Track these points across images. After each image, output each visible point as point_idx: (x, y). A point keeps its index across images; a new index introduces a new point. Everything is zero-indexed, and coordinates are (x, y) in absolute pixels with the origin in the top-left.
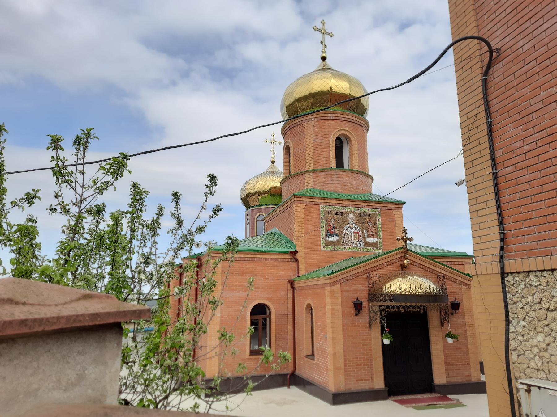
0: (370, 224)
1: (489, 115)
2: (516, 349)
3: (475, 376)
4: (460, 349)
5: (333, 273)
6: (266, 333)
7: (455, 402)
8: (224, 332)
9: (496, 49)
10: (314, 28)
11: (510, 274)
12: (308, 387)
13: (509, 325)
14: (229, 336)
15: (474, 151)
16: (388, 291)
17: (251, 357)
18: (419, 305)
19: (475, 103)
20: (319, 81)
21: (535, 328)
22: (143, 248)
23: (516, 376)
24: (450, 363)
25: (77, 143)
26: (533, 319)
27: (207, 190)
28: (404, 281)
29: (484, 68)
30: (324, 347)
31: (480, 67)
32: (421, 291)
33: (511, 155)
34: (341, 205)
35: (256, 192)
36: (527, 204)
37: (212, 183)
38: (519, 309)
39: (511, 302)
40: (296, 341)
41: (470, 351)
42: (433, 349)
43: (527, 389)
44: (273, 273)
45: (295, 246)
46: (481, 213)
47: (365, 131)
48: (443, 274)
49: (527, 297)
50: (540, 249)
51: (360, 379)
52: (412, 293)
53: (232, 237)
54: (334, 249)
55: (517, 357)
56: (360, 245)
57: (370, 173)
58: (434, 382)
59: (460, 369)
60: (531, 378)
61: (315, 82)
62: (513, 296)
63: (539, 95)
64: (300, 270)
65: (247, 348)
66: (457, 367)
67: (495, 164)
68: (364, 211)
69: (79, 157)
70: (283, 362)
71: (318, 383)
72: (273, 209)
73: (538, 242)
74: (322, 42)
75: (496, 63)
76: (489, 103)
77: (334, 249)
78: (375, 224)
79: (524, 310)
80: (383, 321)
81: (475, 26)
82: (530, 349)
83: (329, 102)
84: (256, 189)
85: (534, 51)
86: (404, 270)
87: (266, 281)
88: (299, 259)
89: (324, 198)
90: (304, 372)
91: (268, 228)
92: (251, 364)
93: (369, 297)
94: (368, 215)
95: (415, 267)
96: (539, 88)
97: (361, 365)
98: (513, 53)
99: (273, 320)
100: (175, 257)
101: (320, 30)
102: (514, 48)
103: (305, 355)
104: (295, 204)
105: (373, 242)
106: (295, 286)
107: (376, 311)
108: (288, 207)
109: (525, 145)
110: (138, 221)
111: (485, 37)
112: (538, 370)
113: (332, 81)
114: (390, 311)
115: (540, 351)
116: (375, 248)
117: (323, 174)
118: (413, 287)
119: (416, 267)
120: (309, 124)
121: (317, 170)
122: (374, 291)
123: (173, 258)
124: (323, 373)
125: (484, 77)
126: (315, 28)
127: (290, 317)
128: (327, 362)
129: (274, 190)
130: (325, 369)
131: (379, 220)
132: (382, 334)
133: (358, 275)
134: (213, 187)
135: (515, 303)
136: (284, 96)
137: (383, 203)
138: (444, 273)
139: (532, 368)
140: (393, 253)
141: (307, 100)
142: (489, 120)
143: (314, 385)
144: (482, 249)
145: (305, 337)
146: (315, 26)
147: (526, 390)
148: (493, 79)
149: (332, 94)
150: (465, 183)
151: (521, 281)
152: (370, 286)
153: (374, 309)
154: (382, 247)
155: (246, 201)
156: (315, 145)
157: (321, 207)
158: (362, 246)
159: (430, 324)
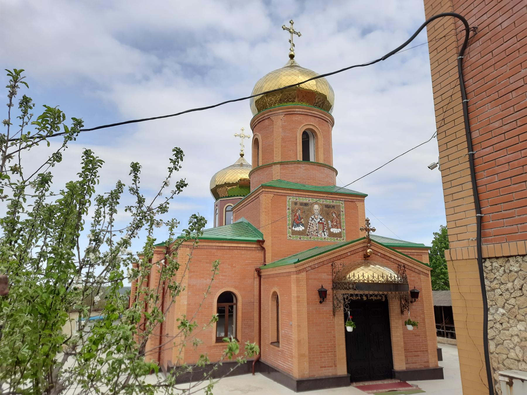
0: (334, 215)
1: (465, 95)
2: (494, 339)
3: (433, 361)
4: (419, 336)
5: (299, 261)
6: (232, 320)
7: (415, 388)
8: (184, 320)
9: (473, 27)
10: (283, 27)
11: (488, 260)
12: (273, 374)
13: (487, 313)
14: (189, 325)
15: (448, 133)
16: (352, 280)
17: (217, 344)
18: (381, 293)
19: (450, 83)
20: (287, 77)
21: (516, 316)
22: (96, 225)
23: (493, 367)
24: (409, 350)
25: (24, 104)
26: (513, 307)
27: (172, 165)
28: (366, 269)
29: (460, 48)
30: (289, 334)
31: (456, 47)
32: (383, 280)
33: (489, 135)
34: (307, 196)
35: (226, 184)
36: (507, 186)
37: (178, 158)
38: (497, 296)
39: (489, 289)
40: (262, 329)
41: (428, 338)
42: (393, 336)
43: (508, 381)
44: (240, 261)
45: (262, 235)
46: (456, 196)
47: (330, 126)
48: (404, 263)
49: (507, 283)
50: (520, 232)
51: (323, 366)
52: (375, 282)
53: (197, 215)
54: (300, 238)
55: (495, 346)
56: (325, 235)
57: (334, 166)
58: (394, 368)
59: (418, 356)
60: (511, 369)
61: (284, 78)
62: (491, 282)
63: (520, 73)
64: (266, 258)
65: (213, 336)
66: (416, 354)
67: (472, 146)
68: (329, 202)
69: (24, 121)
70: (250, 355)
71: (283, 370)
72: (242, 200)
73: (519, 225)
74: (290, 41)
75: (472, 43)
76: (465, 83)
77: (300, 238)
78: (339, 216)
79: (503, 297)
80: (346, 309)
81: (450, 6)
82: (510, 338)
83: (297, 97)
84: (225, 181)
85: (514, 28)
86: (367, 259)
87: (233, 269)
88: (265, 248)
89: (291, 190)
90: (269, 359)
91: (236, 218)
92: (217, 351)
93: (333, 285)
94: (333, 206)
95: (377, 256)
96: (520, 65)
97: (325, 352)
98: (490, 31)
99: (239, 307)
100: (132, 236)
101: (289, 30)
102: (492, 26)
103: (270, 342)
104: (263, 194)
105: (337, 232)
106: (262, 274)
107: (340, 299)
108: (256, 198)
109: (504, 125)
110: (88, 194)
111: (462, 15)
112: (519, 361)
113: (299, 77)
114: (353, 299)
115: (521, 340)
116: (339, 239)
117: (290, 166)
118: (376, 275)
119: (378, 257)
120: (277, 118)
121: (285, 162)
122: (338, 279)
123: (129, 237)
124: (288, 360)
125: (460, 57)
126: (284, 27)
127: (256, 304)
128: (292, 349)
129: (243, 182)
130: (290, 356)
131: (342, 211)
132: (345, 321)
133: (323, 264)
134: (178, 163)
135: (493, 290)
136: (254, 91)
137: (347, 195)
138: (404, 262)
139: (512, 359)
140: (356, 243)
141: (275, 95)
142: (465, 100)
143: (278, 372)
144: (457, 234)
145: (270, 325)
146: (284, 26)
147: (507, 383)
148: (469, 58)
149: (299, 90)
150: (438, 166)
151: (500, 267)
152: (335, 275)
153: (337, 297)
154: (345, 238)
155: (215, 192)
156: (283, 139)
157: (288, 198)
158: (326, 236)
159: (391, 312)
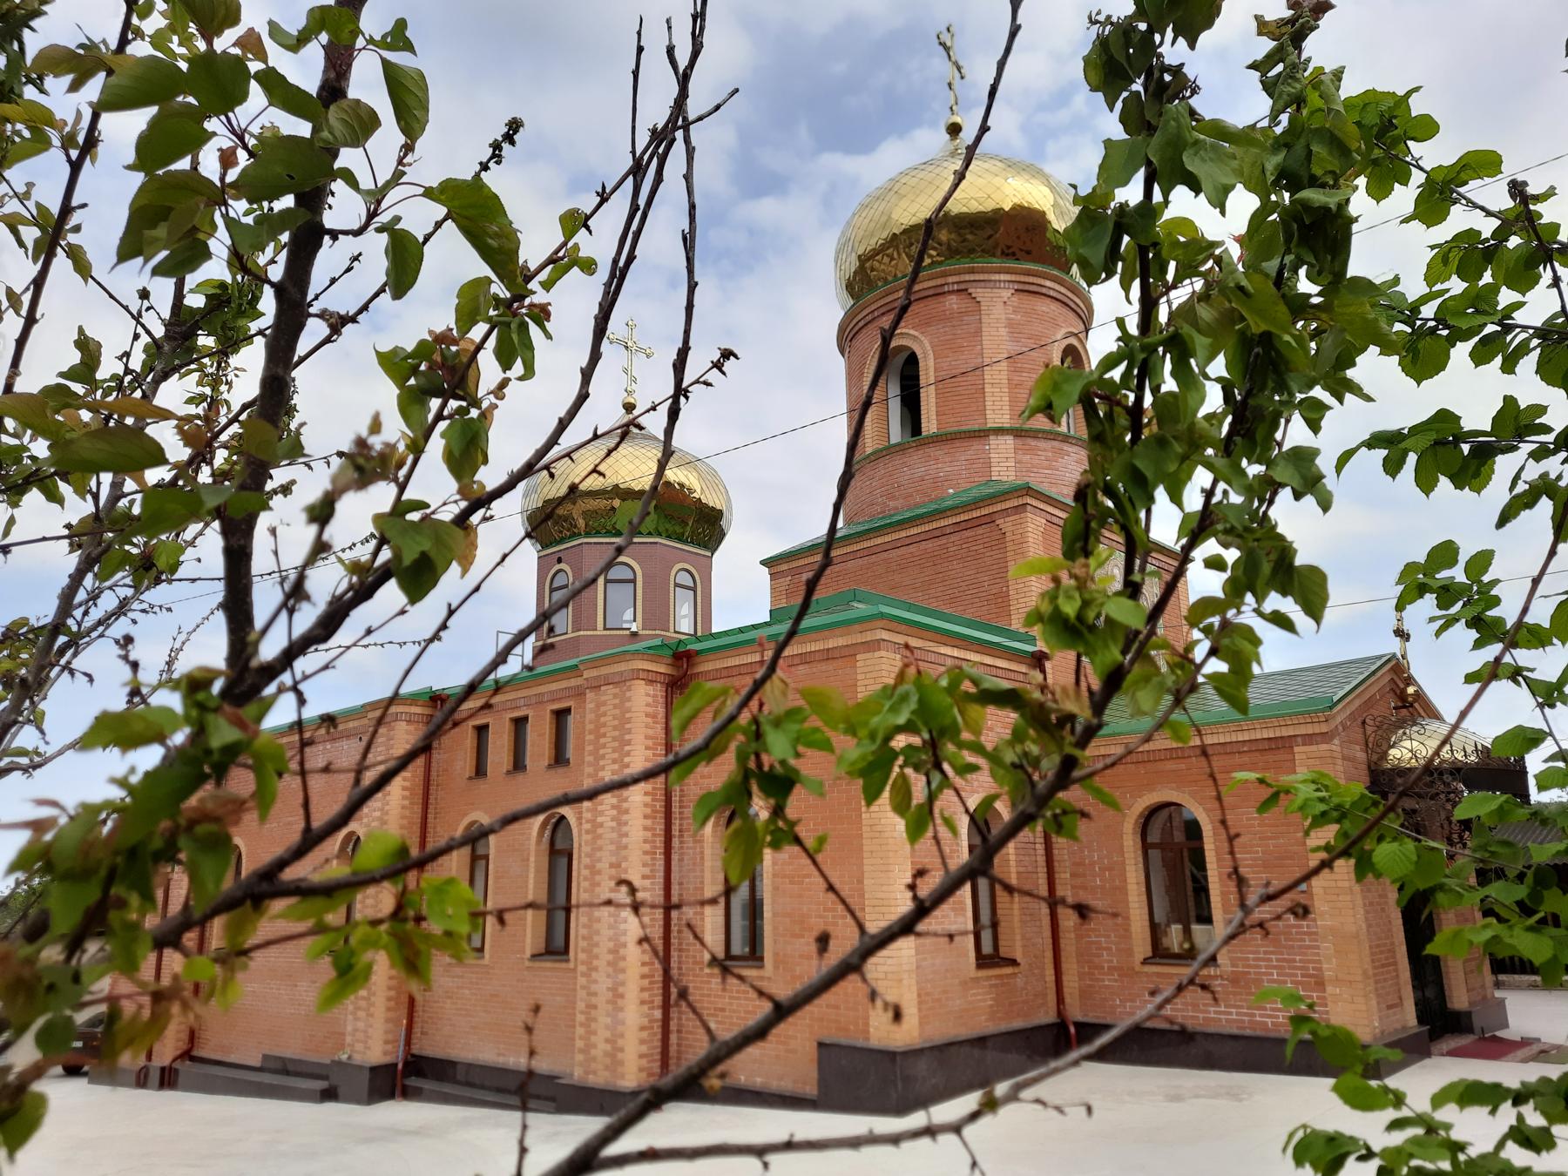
103: (528, 954)
117: (1042, 444)
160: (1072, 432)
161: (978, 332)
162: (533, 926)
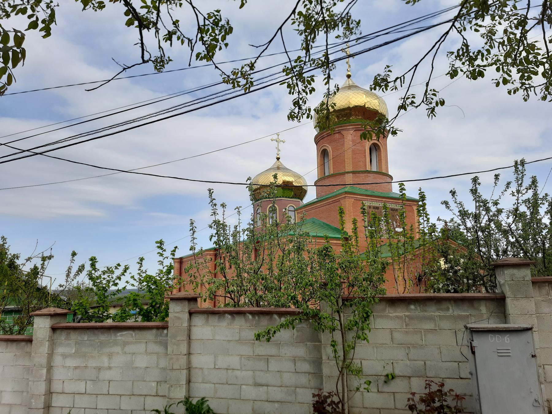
0: (397, 217)
117: (361, 175)
121: (357, 171)
160: (295, 208)
161: (343, 144)
162: (453, 297)
